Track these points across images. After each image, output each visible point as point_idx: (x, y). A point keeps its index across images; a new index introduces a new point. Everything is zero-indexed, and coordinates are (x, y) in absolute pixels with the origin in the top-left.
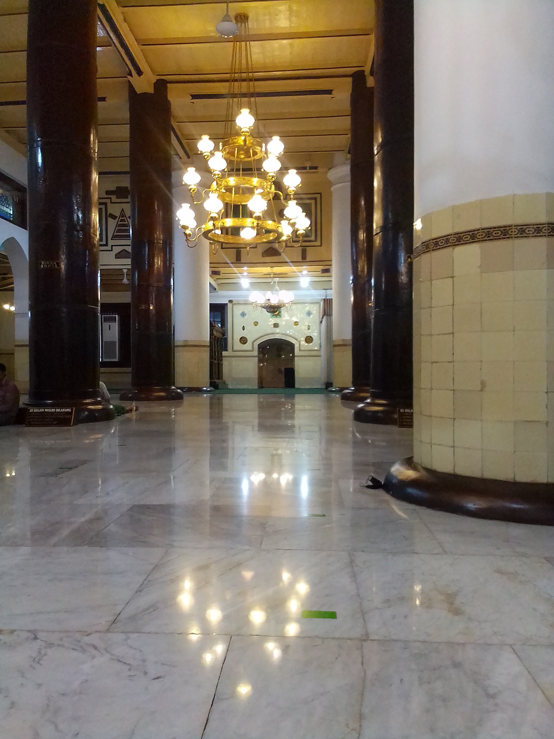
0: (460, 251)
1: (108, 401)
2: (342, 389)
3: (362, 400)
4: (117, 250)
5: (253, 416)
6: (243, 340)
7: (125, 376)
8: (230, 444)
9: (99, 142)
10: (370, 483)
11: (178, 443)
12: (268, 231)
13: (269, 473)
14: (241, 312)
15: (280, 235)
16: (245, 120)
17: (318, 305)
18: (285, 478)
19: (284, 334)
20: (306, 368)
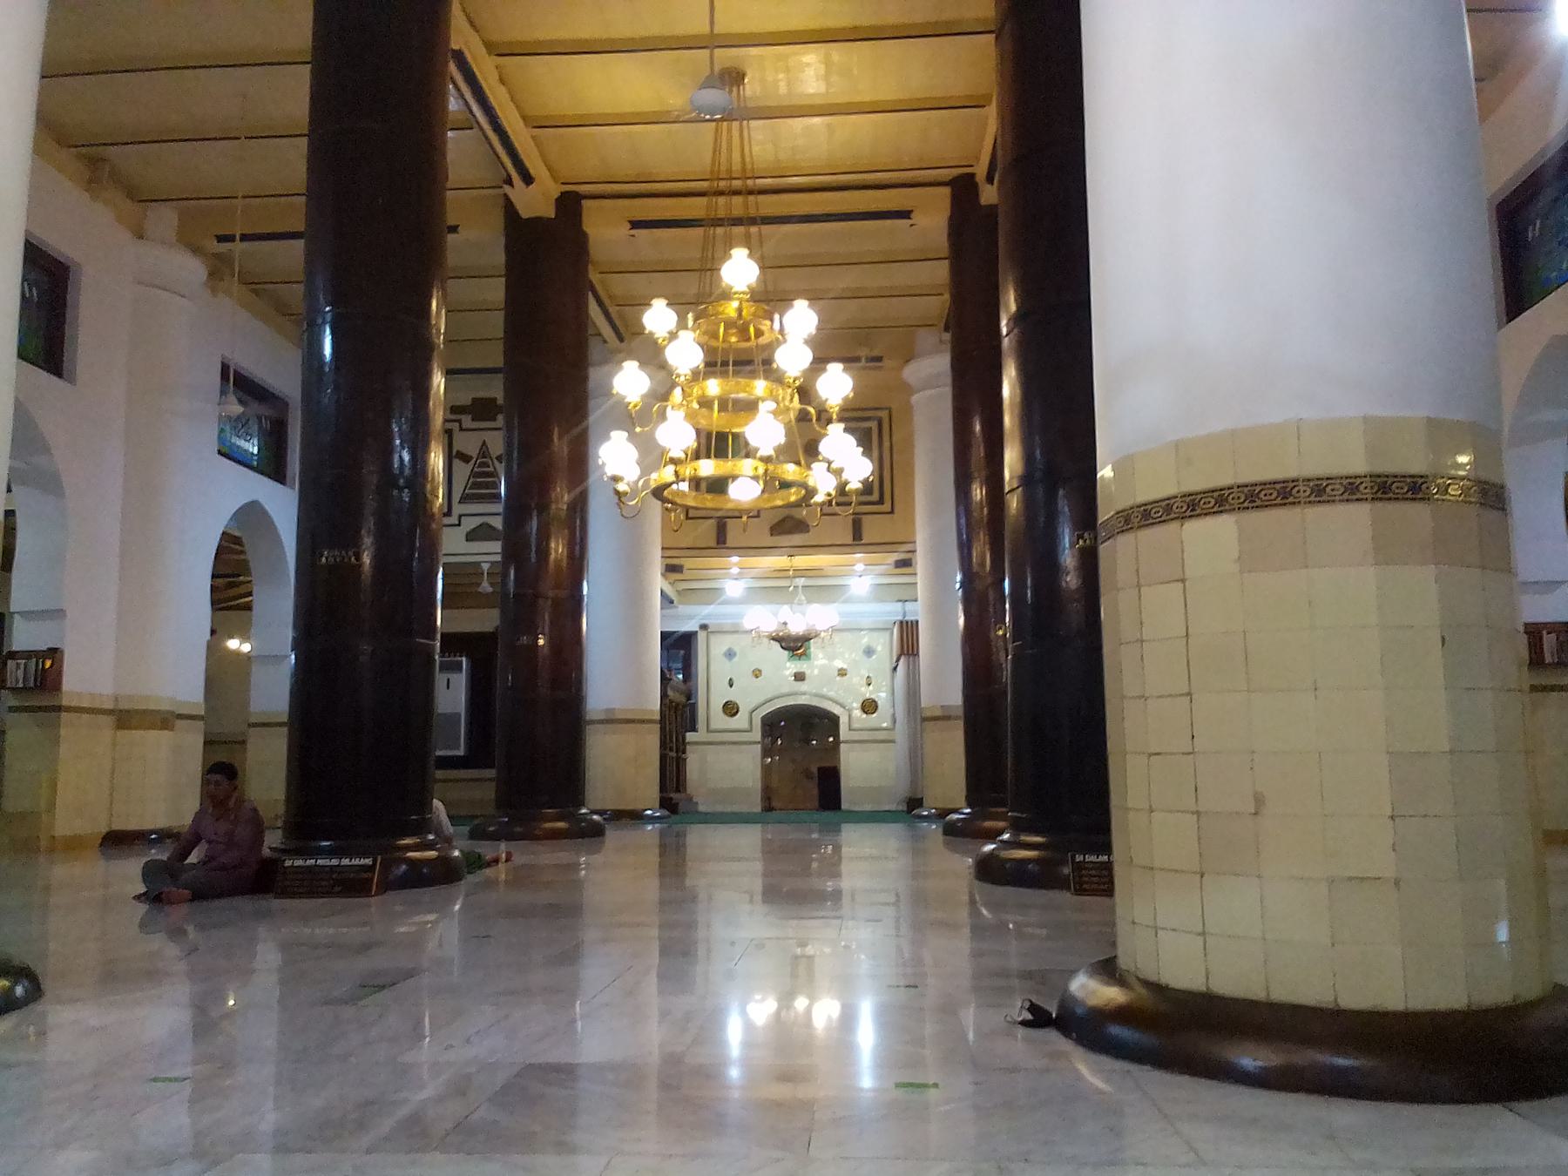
0: (1197, 531)
1: (448, 841)
2: (942, 814)
3: (992, 835)
4: (470, 524)
5: (752, 873)
6: (731, 709)
7: (481, 787)
8: (701, 933)
9: (448, 311)
10: (1030, 1017)
11: (590, 935)
12: (785, 485)
13: (786, 999)
14: (725, 649)
15: (811, 492)
16: (740, 270)
17: (887, 634)
18: (824, 1012)
19: (816, 695)
20: (865, 767)
